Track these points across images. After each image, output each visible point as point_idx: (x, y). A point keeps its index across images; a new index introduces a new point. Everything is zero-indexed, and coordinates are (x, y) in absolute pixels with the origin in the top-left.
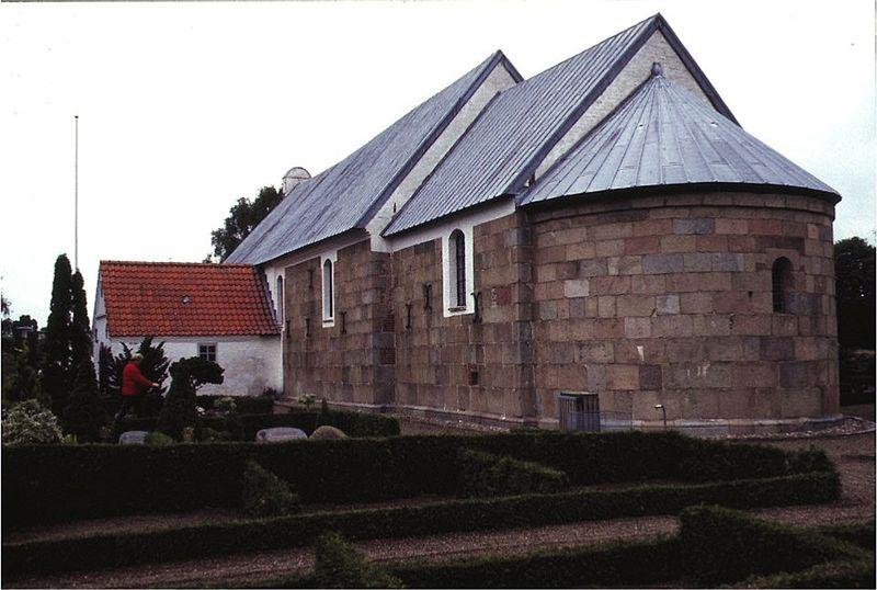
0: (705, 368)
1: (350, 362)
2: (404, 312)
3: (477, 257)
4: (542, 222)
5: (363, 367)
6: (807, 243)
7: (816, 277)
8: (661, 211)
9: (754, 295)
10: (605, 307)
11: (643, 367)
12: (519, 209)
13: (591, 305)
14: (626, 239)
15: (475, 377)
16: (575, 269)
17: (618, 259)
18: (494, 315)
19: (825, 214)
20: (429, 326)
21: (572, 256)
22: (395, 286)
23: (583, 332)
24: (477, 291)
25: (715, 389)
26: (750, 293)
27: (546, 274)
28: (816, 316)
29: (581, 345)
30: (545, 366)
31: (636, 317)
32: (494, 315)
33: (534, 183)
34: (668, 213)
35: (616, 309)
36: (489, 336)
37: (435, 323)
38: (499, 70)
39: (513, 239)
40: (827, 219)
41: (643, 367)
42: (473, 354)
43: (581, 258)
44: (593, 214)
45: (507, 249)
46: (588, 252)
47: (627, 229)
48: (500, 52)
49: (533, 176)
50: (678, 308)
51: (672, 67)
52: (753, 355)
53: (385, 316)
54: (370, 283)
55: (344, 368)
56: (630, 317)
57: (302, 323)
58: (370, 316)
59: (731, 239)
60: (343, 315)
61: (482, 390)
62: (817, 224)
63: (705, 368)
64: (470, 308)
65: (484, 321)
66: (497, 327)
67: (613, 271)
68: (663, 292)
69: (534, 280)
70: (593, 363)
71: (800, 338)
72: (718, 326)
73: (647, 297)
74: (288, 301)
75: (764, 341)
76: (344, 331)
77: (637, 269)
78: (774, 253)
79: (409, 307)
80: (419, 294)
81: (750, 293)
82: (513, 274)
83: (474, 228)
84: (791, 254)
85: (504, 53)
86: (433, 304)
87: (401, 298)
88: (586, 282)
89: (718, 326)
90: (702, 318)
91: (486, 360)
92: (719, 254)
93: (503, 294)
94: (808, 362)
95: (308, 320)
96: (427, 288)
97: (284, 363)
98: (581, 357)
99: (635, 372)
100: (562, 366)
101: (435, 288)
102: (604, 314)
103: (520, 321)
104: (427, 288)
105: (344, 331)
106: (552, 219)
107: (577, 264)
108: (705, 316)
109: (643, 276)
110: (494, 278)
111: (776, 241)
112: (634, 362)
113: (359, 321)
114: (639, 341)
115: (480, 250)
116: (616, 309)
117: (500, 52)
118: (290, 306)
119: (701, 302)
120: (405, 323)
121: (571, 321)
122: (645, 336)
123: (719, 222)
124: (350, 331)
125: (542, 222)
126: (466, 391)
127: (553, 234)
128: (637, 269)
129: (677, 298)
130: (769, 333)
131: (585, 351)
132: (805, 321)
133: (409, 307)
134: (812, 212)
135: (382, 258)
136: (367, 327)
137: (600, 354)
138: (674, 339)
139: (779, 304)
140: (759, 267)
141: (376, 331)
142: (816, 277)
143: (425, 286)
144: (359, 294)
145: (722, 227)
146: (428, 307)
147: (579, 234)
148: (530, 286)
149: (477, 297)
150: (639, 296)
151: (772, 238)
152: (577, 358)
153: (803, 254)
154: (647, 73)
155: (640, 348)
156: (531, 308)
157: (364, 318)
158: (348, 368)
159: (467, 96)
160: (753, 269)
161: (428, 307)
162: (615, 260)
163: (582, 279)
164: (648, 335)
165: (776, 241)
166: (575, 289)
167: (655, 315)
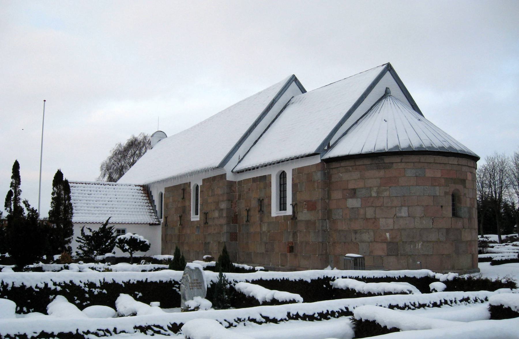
0: (420, 244)
1: (209, 239)
2: (245, 213)
3: (294, 186)
4: (335, 168)
5: (219, 242)
6: (467, 181)
7: (470, 199)
8: (399, 164)
9: (443, 207)
10: (370, 212)
11: (389, 243)
12: (322, 160)
13: (362, 211)
14: (381, 178)
15: (291, 249)
16: (354, 193)
17: (377, 188)
18: (304, 215)
19: (474, 167)
20: (261, 221)
21: (351, 186)
22: (239, 199)
23: (356, 226)
24: (294, 203)
25: (425, 255)
26: (442, 207)
27: (337, 195)
28: (470, 218)
29: (356, 232)
30: (334, 243)
31: (386, 218)
32: (304, 215)
33: (330, 148)
34: (403, 165)
35: (375, 214)
36: (302, 227)
37: (266, 219)
38: (294, 85)
39: (318, 176)
40: (474, 169)
41: (389, 243)
42: (291, 236)
43: (356, 187)
44: (364, 165)
45: (314, 182)
46: (361, 184)
47: (382, 173)
48: (294, 76)
49: (329, 144)
50: (407, 214)
51: (395, 90)
52: (443, 238)
53: (233, 216)
54: (225, 198)
55: (205, 243)
56: (383, 218)
57: (176, 218)
58: (224, 215)
59: (434, 179)
60: (206, 215)
61: (296, 255)
62: (471, 173)
63: (420, 244)
64: (289, 211)
65: (299, 219)
66: (308, 222)
67: (374, 194)
68: (400, 205)
69: (329, 198)
70: (363, 242)
71: (464, 229)
72: (427, 223)
73: (392, 207)
74: (167, 205)
75: (448, 230)
76: (206, 223)
77: (386, 194)
78: (452, 187)
79: (248, 211)
80: (254, 203)
81: (442, 207)
82: (317, 195)
83: (293, 170)
84: (459, 187)
85: (296, 76)
86: (265, 209)
87: (242, 206)
88: (359, 200)
89: (427, 223)
90: (419, 219)
91: (299, 240)
92: (427, 187)
93: (311, 206)
94: (467, 242)
95: (181, 217)
96: (261, 202)
97: (162, 240)
98: (356, 238)
99: (385, 246)
100: (345, 243)
101: (266, 201)
102: (368, 216)
103: (322, 219)
104: (261, 202)
105: (206, 223)
106: (341, 167)
107: (354, 191)
108: (420, 218)
109: (389, 197)
110: (305, 196)
111: (455, 181)
112: (384, 241)
113: (217, 218)
114: (387, 231)
115: (297, 181)
116: (375, 214)
117: (294, 76)
118: (167, 208)
119: (418, 211)
120: (245, 219)
121: (351, 220)
122: (390, 228)
123: (427, 170)
124: (210, 223)
125: (335, 168)
126: (285, 256)
127: (341, 175)
128: (386, 194)
129: (406, 208)
130: (450, 227)
131: (358, 236)
132: (466, 221)
133: (248, 211)
134: (469, 167)
135: (231, 184)
136: (223, 221)
137: (366, 237)
138: (404, 230)
139: (455, 214)
140: (446, 193)
141: (228, 223)
142: (470, 199)
143: (259, 200)
144: (217, 203)
145: (429, 174)
146: (261, 210)
147: (356, 175)
148: (327, 201)
149: (294, 206)
150: (388, 207)
151: (452, 179)
152: (353, 239)
153: (465, 187)
154: (383, 93)
155: (388, 235)
156: (328, 213)
157: (220, 216)
158: (209, 243)
159: (277, 99)
160: (443, 194)
161: (261, 210)
162: (375, 189)
163: (357, 198)
164: (392, 228)
165: (455, 181)
166: (353, 203)
167: (395, 217)
